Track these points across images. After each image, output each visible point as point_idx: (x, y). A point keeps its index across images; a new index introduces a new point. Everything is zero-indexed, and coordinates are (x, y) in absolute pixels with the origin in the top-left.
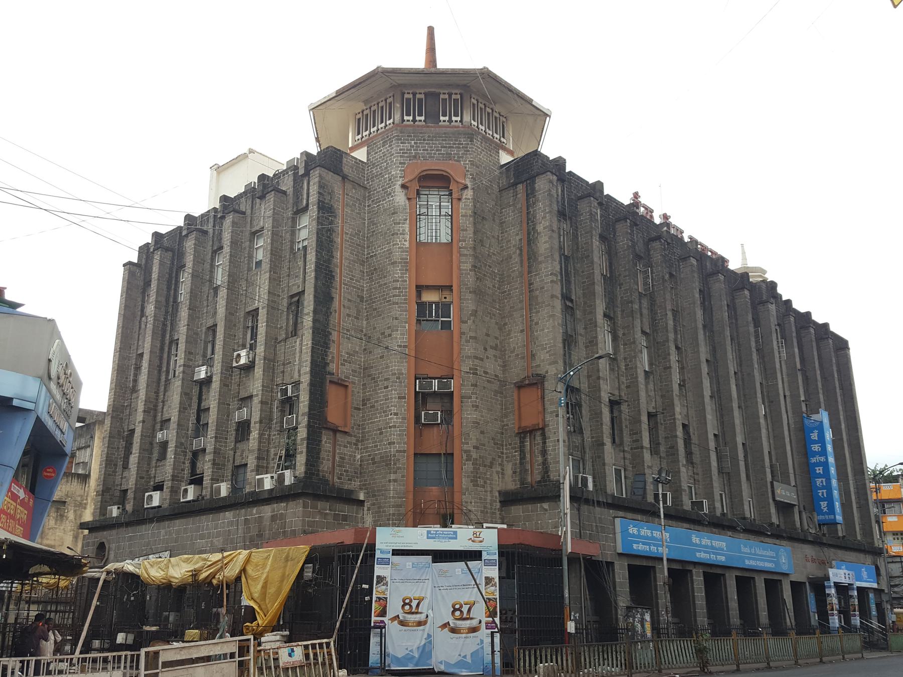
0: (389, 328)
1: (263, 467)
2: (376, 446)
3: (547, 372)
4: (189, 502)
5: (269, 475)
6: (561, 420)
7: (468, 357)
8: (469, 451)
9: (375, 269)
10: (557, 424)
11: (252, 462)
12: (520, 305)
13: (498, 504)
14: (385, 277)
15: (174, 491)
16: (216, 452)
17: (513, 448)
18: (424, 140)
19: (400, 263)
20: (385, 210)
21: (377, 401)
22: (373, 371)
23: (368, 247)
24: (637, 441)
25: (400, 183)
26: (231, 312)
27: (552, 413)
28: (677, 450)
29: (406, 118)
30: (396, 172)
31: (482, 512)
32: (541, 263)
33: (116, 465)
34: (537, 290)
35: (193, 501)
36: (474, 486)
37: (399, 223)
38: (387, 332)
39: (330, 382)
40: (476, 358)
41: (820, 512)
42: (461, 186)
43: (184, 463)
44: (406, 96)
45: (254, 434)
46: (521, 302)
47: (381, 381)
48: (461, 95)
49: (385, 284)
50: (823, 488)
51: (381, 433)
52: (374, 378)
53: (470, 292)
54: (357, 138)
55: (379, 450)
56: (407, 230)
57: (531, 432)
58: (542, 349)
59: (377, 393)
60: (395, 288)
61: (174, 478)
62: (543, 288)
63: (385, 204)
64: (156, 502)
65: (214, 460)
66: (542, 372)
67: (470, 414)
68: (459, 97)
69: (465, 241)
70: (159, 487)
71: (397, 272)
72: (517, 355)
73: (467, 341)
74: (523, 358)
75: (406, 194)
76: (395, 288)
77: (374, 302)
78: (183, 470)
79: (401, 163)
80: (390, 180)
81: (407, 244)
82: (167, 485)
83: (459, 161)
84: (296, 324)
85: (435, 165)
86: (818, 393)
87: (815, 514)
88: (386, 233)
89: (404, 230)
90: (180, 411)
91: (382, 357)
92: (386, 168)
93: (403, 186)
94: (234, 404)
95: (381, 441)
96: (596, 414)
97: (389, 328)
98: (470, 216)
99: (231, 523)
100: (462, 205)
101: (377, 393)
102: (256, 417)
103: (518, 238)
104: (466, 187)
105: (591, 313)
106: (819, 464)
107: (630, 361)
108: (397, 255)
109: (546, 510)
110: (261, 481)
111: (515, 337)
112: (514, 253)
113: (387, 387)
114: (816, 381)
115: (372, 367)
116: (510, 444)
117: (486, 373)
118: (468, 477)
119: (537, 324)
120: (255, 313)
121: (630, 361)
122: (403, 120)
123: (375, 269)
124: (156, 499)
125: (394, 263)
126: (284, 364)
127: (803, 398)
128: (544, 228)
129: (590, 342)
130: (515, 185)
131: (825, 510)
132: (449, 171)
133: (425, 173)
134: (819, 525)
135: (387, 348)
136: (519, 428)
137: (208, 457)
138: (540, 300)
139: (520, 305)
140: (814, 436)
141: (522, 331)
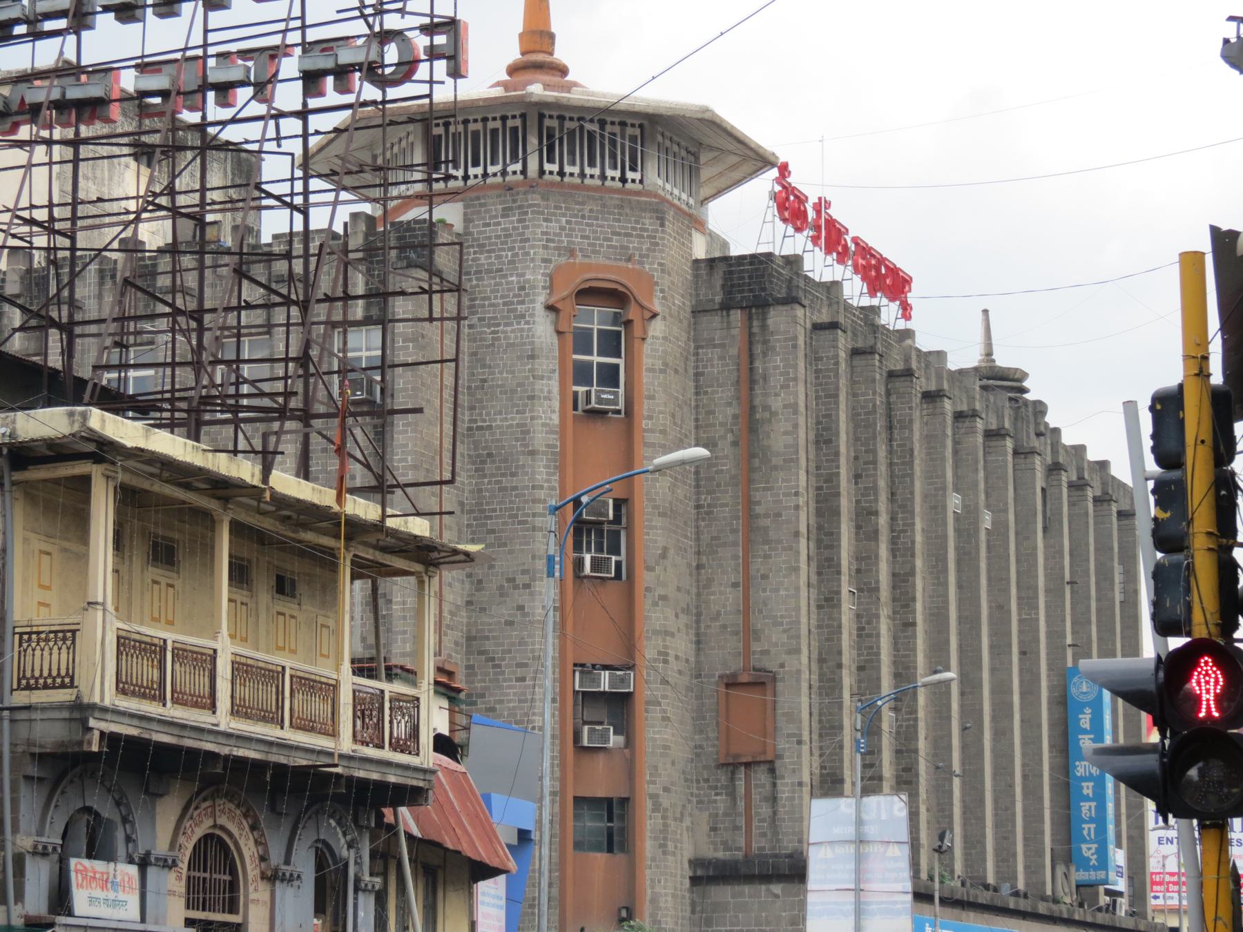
0: (524, 572)
3: (782, 666)
6: (805, 748)
7: (656, 632)
8: (657, 796)
9: (490, 455)
10: (799, 756)
12: (731, 538)
13: (687, 881)
14: (513, 475)
17: (711, 788)
18: (583, 217)
19: (544, 453)
20: (509, 345)
21: (501, 702)
22: (489, 646)
23: (472, 408)
24: (871, 766)
25: (541, 299)
27: (789, 736)
28: (917, 775)
30: (536, 276)
31: (674, 896)
32: (776, 468)
34: (767, 516)
36: (664, 853)
37: (542, 378)
38: (521, 579)
40: (667, 633)
41: (1084, 864)
42: (648, 315)
46: (734, 531)
47: (507, 666)
49: (515, 488)
50: (1091, 820)
52: (493, 659)
53: (660, 515)
56: (556, 390)
57: (747, 765)
58: (776, 624)
59: (501, 688)
60: (539, 501)
62: (779, 515)
63: (511, 332)
66: (772, 665)
67: (659, 732)
68: (637, 132)
69: (650, 418)
71: (542, 471)
72: (724, 627)
73: (655, 604)
74: (737, 633)
75: (556, 323)
76: (539, 501)
77: (490, 518)
79: (545, 261)
80: (522, 288)
81: (556, 419)
83: (641, 263)
85: (602, 266)
86: (1089, 622)
87: (1073, 869)
88: (514, 391)
89: (549, 392)
91: (510, 623)
92: (512, 262)
93: (551, 308)
96: (832, 727)
97: (524, 572)
98: (661, 371)
100: (647, 348)
103: (730, 411)
104: (655, 315)
105: (830, 547)
106: (1090, 778)
107: (868, 623)
108: (541, 438)
109: (777, 896)
111: (721, 593)
112: (723, 437)
113: (523, 679)
114: (1088, 598)
115: (487, 638)
116: (707, 781)
117: (677, 658)
118: (655, 839)
119: (765, 577)
121: (868, 623)
122: (542, 172)
123: (490, 455)
125: (533, 453)
127: (1069, 641)
128: (785, 407)
129: (826, 600)
130: (726, 307)
131: (1093, 862)
132: (630, 285)
133: (587, 285)
134: (1078, 886)
135: (521, 608)
136: (728, 754)
138: (772, 535)
139: (731, 538)
140: (1085, 721)
141: (735, 585)
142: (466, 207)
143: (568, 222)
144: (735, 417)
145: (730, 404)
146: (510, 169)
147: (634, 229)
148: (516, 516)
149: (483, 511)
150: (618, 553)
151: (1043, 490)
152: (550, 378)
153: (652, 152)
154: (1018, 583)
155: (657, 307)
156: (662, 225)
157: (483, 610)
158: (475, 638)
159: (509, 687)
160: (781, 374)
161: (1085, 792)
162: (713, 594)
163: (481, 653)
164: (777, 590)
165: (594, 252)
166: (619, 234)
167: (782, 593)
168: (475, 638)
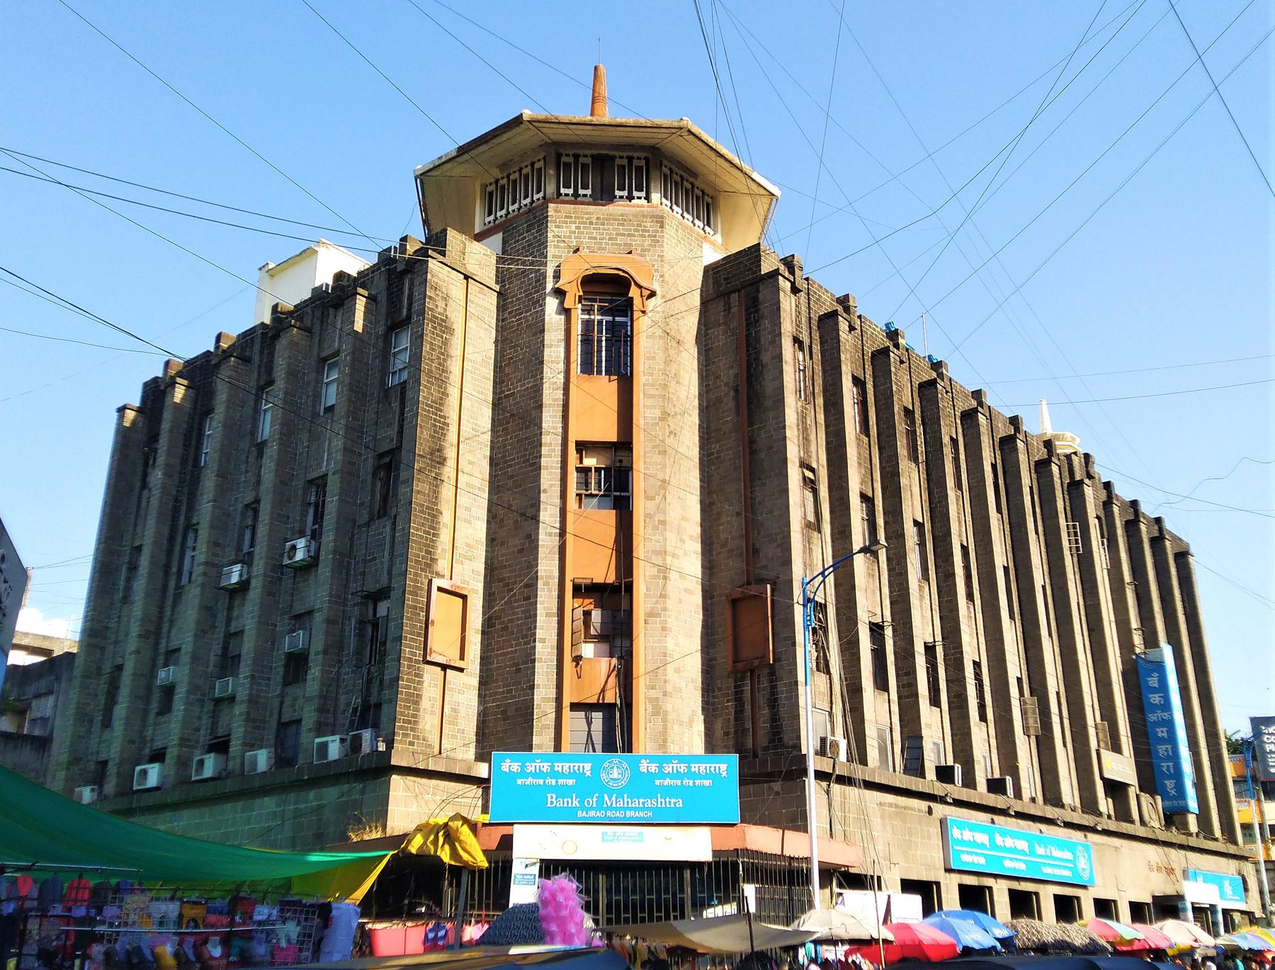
1: (327, 725)
2: (509, 691)
4: (206, 780)
5: (337, 737)
11: (309, 717)
15: (183, 763)
16: (253, 701)
18: (591, 223)
26: (283, 482)
29: (563, 191)
33: (91, 721)
35: (211, 779)
39: (440, 589)
42: (646, 293)
43: (199, 718)
44: (564, 159)
45: (315, 672)
48: (647, 159)
51: (518, 671)
54: (487, 219)
55: (514, 697)
61: (184, 742)
64: (153, 780)
65: (248, 714)
68: (643, 163)
70: (158, 756)
72: (732, 550)
77: (511, 466)
78: (198, 730)
82: (172, 753)
84: (385, 499)
85: (607, 261)
90: (196, 636)
94: (282, 624)
95: (518, 683)
99: (274, 815)
101: (513, 608)
102: (318, 644)
103: (732, 372)
104: (653, 294)
110: (324, 746)
120: (320, 483)
124: (153, 775)
126: (365, 561)
137: (239, 709)
141: (738, 514)
142: (709, 864)
143: (578, 228)
144: (736, 376)
145: (732, 367)
146: (517, 175)
147: (636, 230)
148: (527, 461)
149: (506, 462)
150: (613, 158)
151: (107, 724)
152: (557, 346)
153: (655, 174)
154: (1042, 515)
155: (656, 287)
156: (662, 227)
157: (502, 544)
158: (496, 569)
159: (519, 607)
160: (770, 333)
161: (1160, 735)
162: (722, 524)
163: (500, 580)
164: (772, 512)
165: (599, 249)
166: (623, 235)
167: (776, 513)
168: (496, 569)
